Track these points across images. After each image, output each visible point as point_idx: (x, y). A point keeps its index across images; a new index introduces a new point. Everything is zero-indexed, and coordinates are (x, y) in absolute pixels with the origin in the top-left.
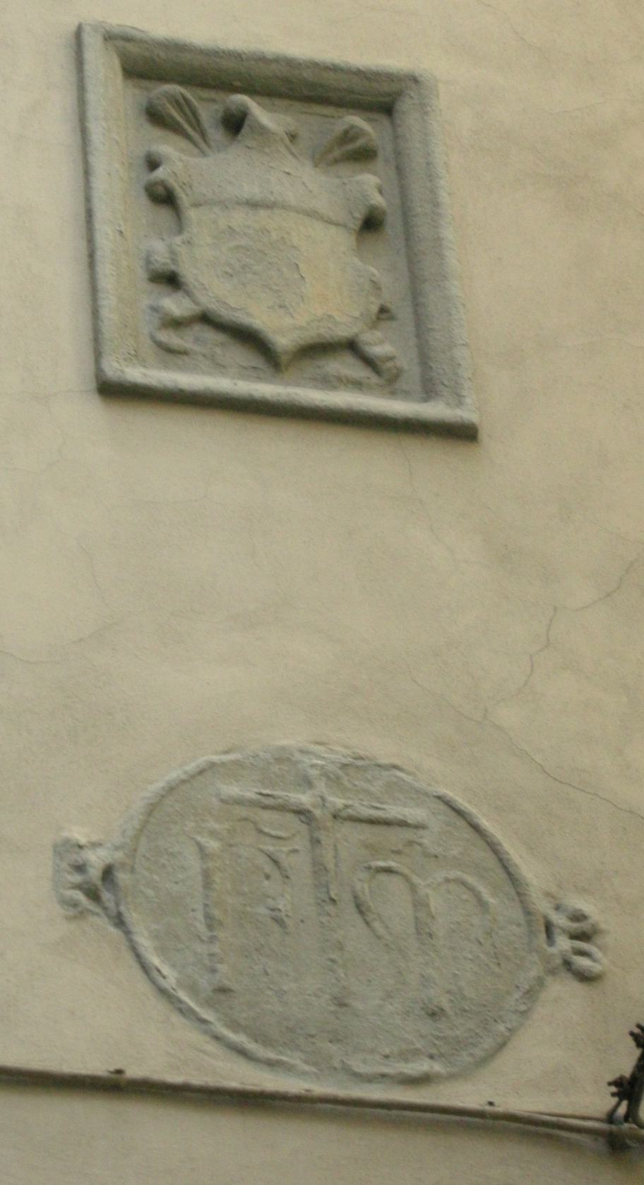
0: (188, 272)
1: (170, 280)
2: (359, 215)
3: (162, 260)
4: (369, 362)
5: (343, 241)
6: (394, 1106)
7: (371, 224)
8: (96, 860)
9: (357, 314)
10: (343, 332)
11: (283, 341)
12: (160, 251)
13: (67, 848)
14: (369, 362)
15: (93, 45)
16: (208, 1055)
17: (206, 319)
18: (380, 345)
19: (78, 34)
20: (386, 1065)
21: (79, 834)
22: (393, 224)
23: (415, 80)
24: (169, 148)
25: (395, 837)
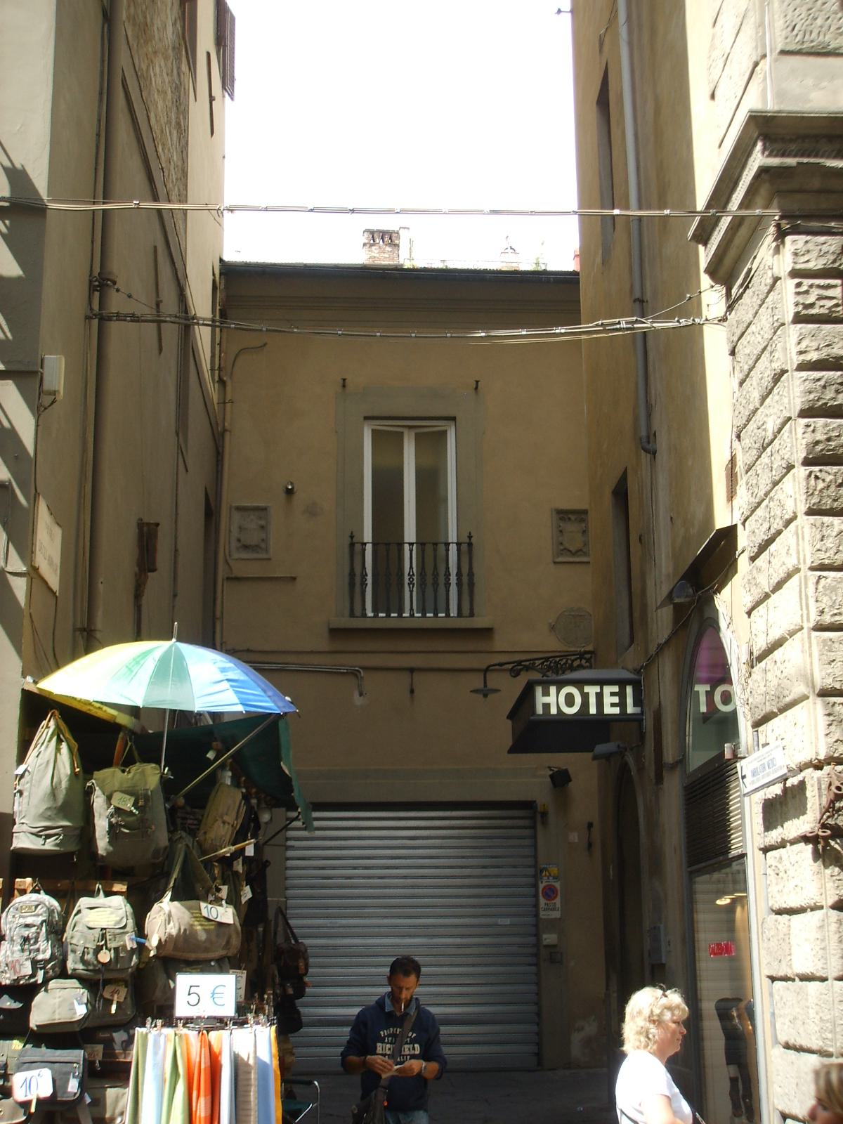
7: (584, 532)
12: (561, 539)
15: (557, 560)
17: (565, 549)
18: (584, 550)
21: (551, 621)
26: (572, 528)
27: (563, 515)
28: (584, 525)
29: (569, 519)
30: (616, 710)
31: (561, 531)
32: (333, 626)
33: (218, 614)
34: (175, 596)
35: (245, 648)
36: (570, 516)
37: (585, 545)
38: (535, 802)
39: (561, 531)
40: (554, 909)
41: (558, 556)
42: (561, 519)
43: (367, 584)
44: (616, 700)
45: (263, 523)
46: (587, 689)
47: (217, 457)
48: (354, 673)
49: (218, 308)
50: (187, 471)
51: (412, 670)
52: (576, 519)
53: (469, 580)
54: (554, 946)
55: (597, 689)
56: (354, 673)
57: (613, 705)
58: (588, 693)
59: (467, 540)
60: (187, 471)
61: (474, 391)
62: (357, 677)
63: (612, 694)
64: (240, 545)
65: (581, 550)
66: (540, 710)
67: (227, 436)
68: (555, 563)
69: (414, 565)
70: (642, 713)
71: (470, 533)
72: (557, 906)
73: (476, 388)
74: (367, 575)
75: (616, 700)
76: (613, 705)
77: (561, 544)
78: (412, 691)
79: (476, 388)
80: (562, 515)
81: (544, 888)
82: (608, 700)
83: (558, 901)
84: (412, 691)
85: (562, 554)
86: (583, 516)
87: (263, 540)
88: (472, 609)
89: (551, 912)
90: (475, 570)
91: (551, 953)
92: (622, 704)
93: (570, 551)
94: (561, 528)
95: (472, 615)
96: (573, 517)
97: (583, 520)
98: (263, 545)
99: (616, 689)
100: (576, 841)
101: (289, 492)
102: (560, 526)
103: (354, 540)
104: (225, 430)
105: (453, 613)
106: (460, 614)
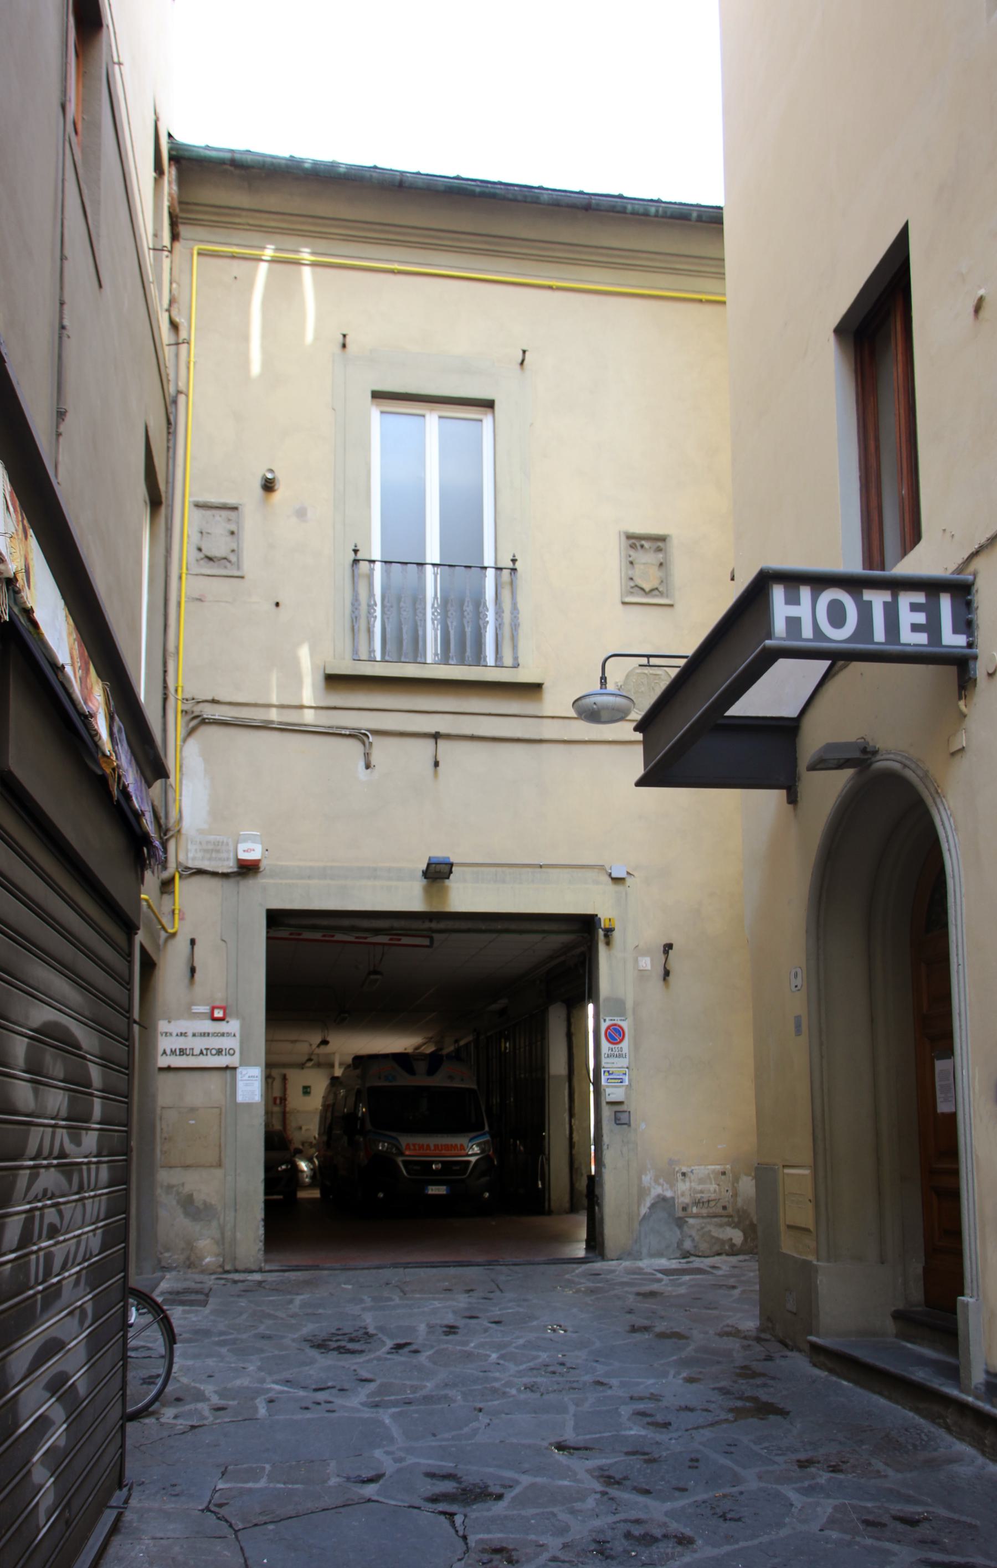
0: (634, 578)
1: (631, 579)
2: (659, 563)
3: (631, 576)
4: (660, 592)
5: (656, 568)
6: (623, 211)
7: (661, 564)
8: (619, 684)
9: (750, 1324)
10: (655, 587)
11: (647, 590)
12: (630, 573)
13: (616, 683)
14: (660, 592)
15: (627, 600)
16: (618, 1483)
17: (637, 586)
18: (661, 589)
19: (624, 603)
20: (624, 203)
21: (617, 680)
22: (664, 564)
23: (668, 536)
24: (632, 552)
25: (657, 677)
26: (646, 559)
27: (635, 541)
28: (660, 556)
29: (642, 546)
30: (922, 638)
31: (631, 563)
32: (329, 671)
33: (171, 647)
34: (59, 435)
35: (210, 698)
36: (643, 542)
37: (662, 582)
38: (597, 915)
39: (631, 563)
40: (620, 1056)
41: (627, 596)
42: (633, 546)
43: (376, 617)
44: (921, 618)
45: (233, 527)
46: (868, 595)
47: (168, 428)
48: (358, 736)
49: (166, 204)
50: (100, 286)
51: (436, 736)
52: (650, 548)
53: (512, 620)
54: (621, 1103)
55: (886, 596)
56: (358, 736)
57: (915, 628)
58: (870, 602)
59: (510, 565)
60: (100, 286)
61: (518, 367)
62: (364, 743)
63: (915, 607)
64: (201, 555)
65: (657, 589)
66: (779, 626)
67: (182, 399)
68: (624, 603)
69: (439, 595)
70: (970, 645)
71: (514, 556)
72: (624, 1052)
73: (522, 363)
74: (376, 605)
75: (921, 618)
76: (915, 628)
77: (631, 579)
78: (436, 764)
79: (522, 363)
80: (633, 541)
81: (608, 1028)
82: (907, 617)
83: (625, 1045)
84: (436, 764)
85: (632, 593)
86: (660, 544)
87: (233, 551)
88: (516, 658)
89: (615, 1060)
90: (520, 606)
91: (616, 1112)
92: (932, 628)
93: (642, 589)
94: (631, 559)
95: (516, 666)
96: (646, 544)
97: (659, 550)
98: (233, 558)
99: (920, 598)
100: (649, 967)
101: (269, 486)
102: (630, 556)
103: (360, 556)
104: (179, 392)
105: (490, 660)
106: (499, 665)
